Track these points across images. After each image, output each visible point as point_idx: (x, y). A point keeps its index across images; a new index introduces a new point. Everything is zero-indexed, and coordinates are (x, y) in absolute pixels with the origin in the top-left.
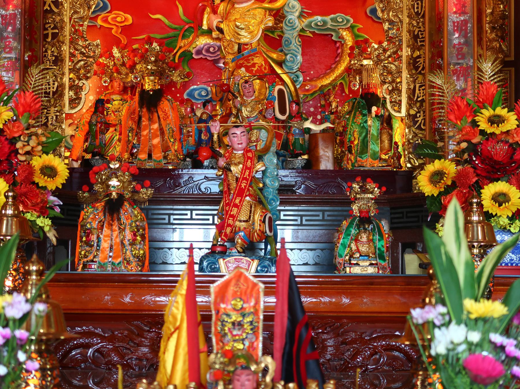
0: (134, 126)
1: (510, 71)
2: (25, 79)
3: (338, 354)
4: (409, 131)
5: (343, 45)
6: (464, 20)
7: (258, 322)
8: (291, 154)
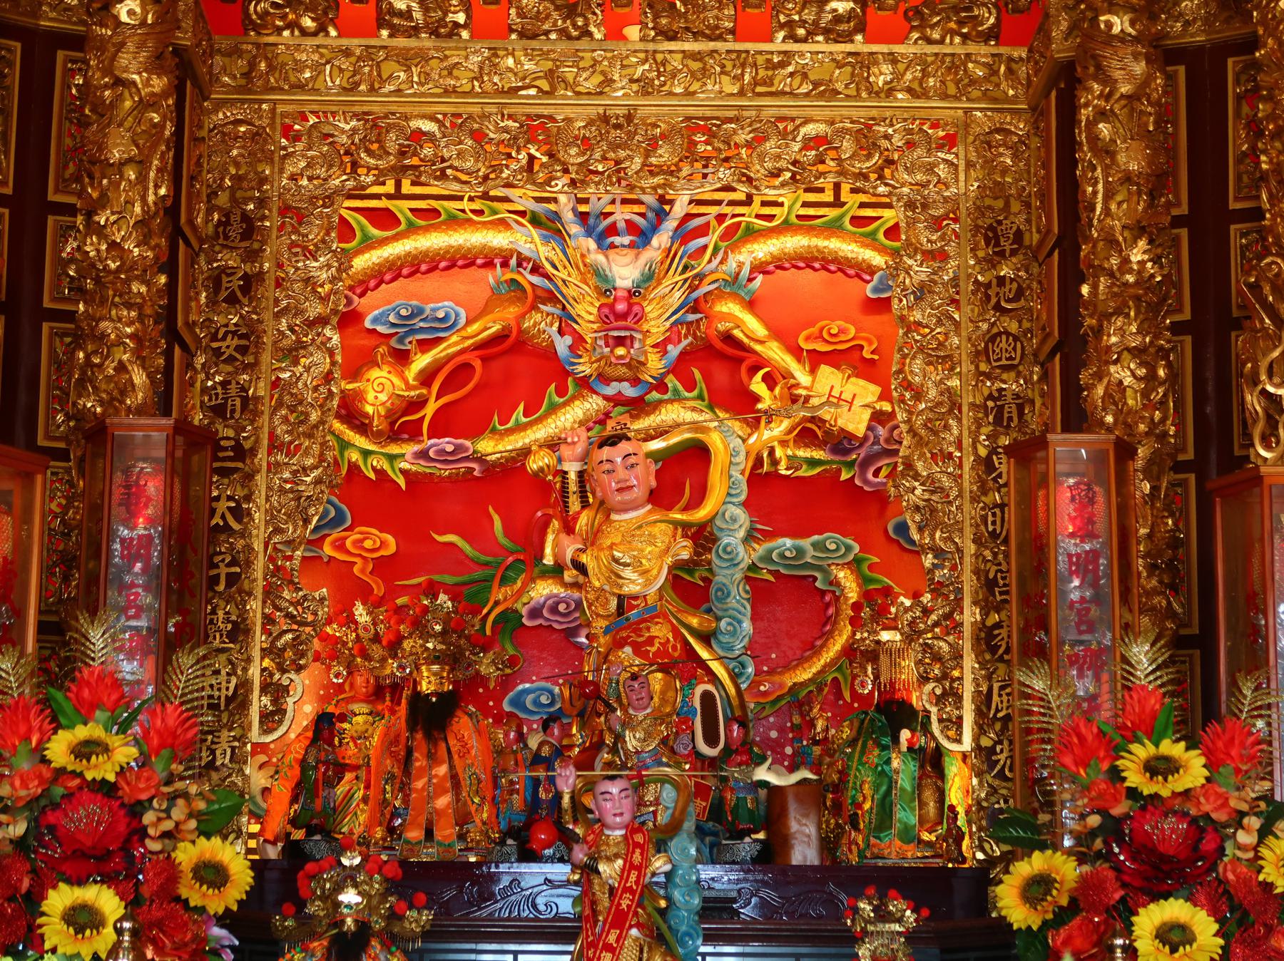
0: (395, 770)
1: (1191, 656)
2: (166, 677)
4: (981, 783)
5: (837, 599)
6: (1091, 551)
8: (728, 830)
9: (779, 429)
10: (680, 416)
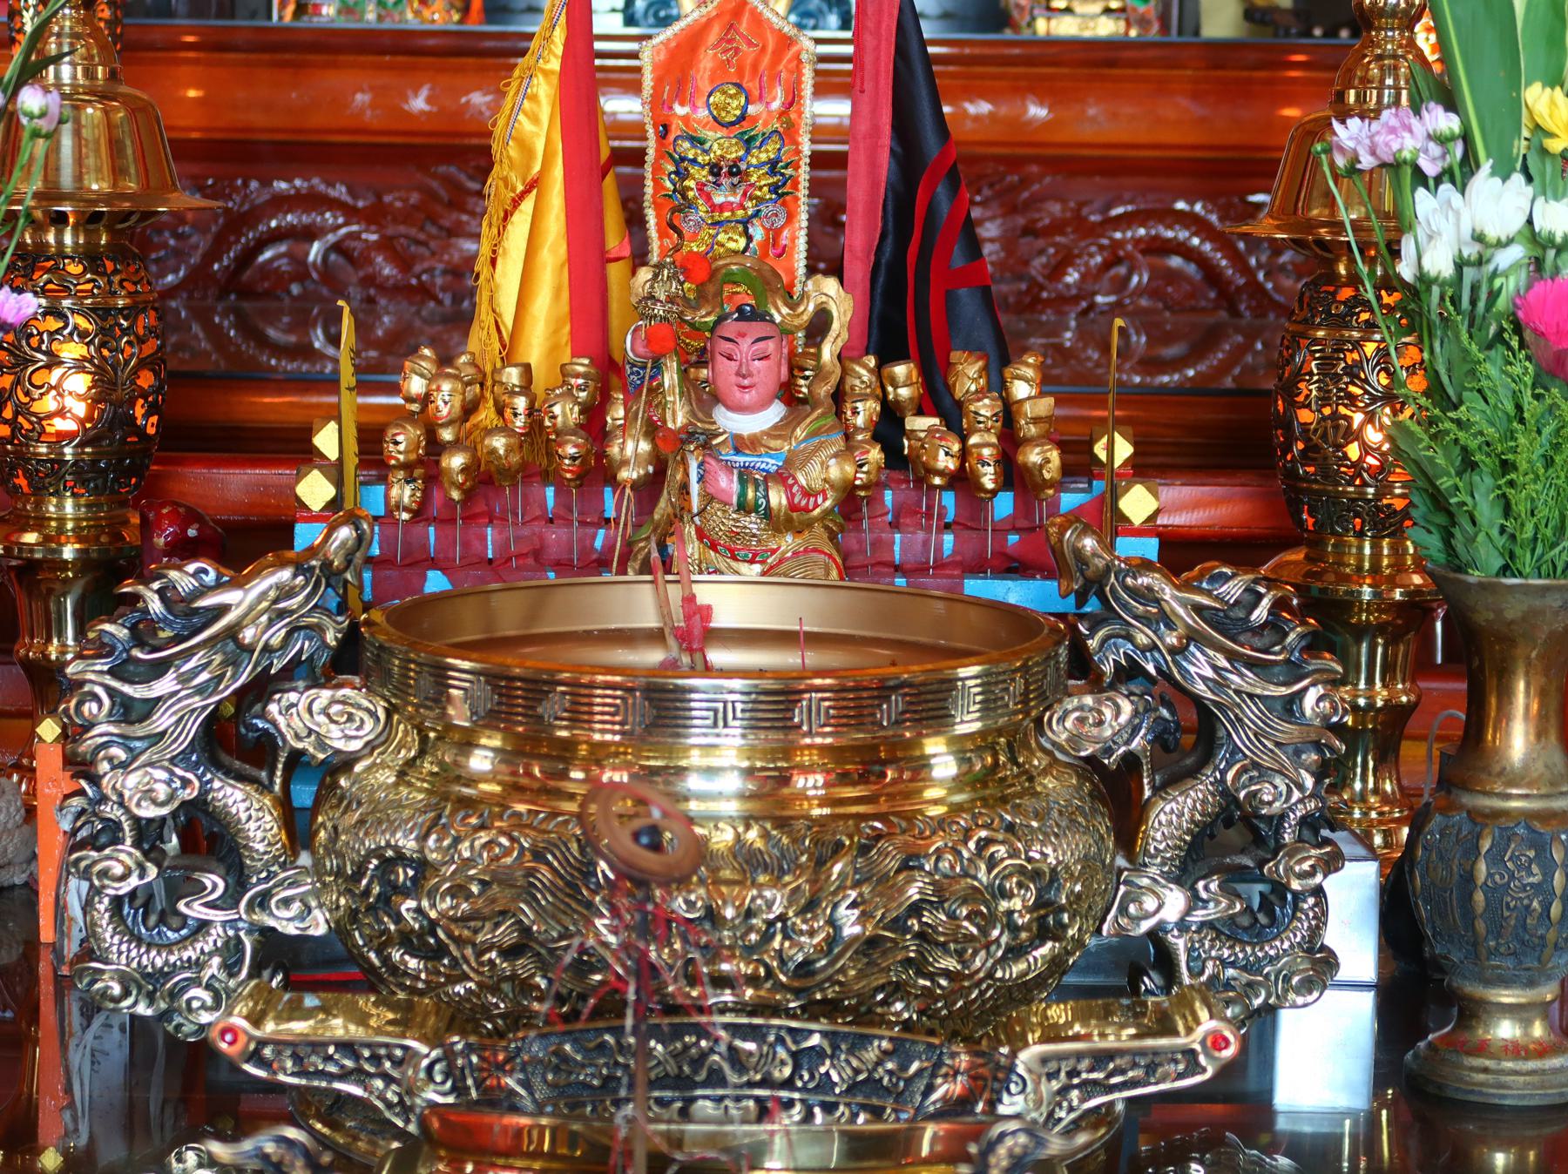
3: (1015, 264)
7: (797, 167)
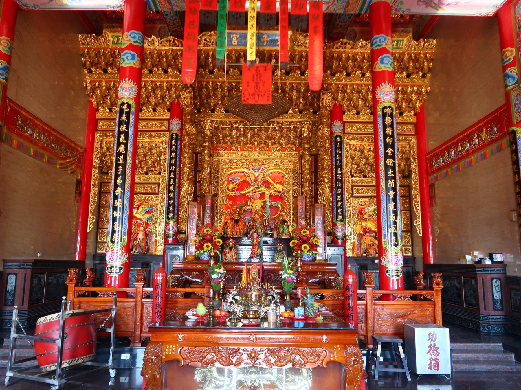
9: (273, 191)
10: (263, 189)
